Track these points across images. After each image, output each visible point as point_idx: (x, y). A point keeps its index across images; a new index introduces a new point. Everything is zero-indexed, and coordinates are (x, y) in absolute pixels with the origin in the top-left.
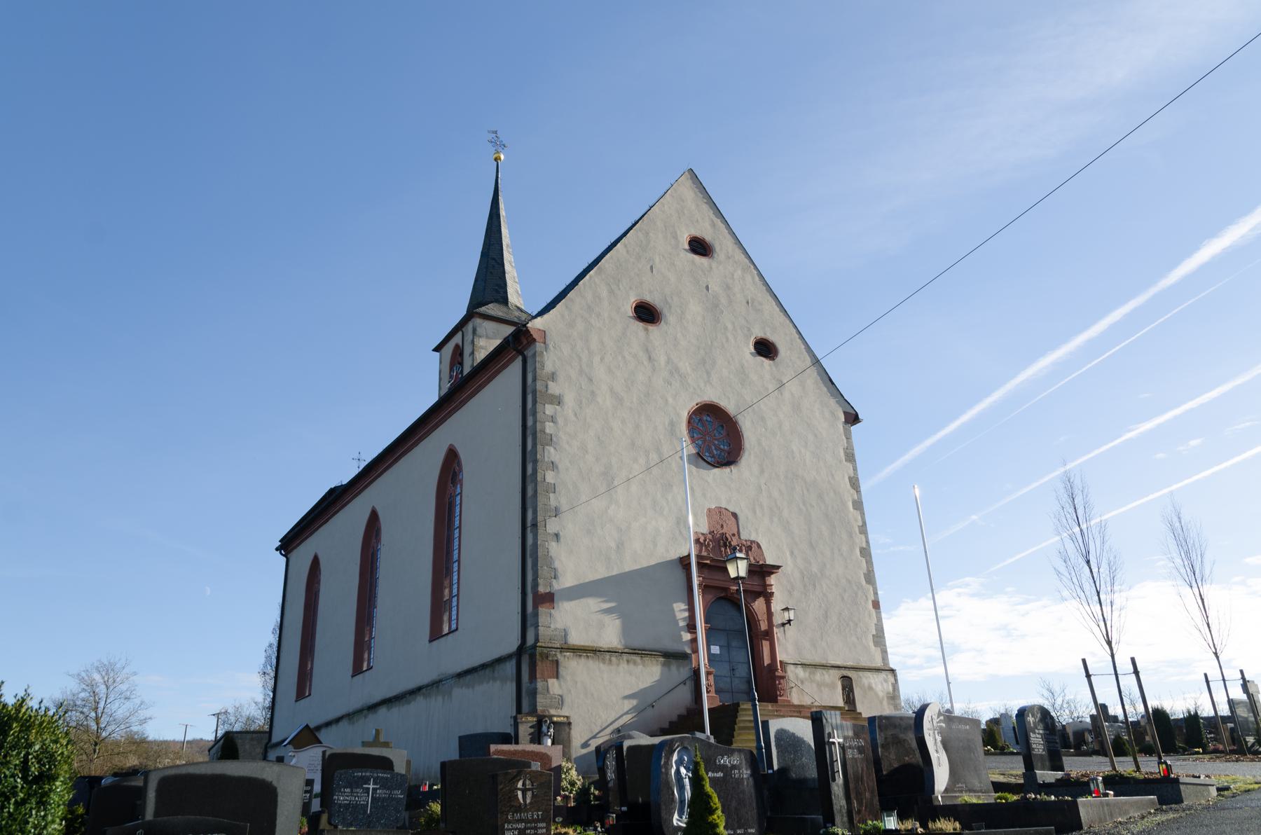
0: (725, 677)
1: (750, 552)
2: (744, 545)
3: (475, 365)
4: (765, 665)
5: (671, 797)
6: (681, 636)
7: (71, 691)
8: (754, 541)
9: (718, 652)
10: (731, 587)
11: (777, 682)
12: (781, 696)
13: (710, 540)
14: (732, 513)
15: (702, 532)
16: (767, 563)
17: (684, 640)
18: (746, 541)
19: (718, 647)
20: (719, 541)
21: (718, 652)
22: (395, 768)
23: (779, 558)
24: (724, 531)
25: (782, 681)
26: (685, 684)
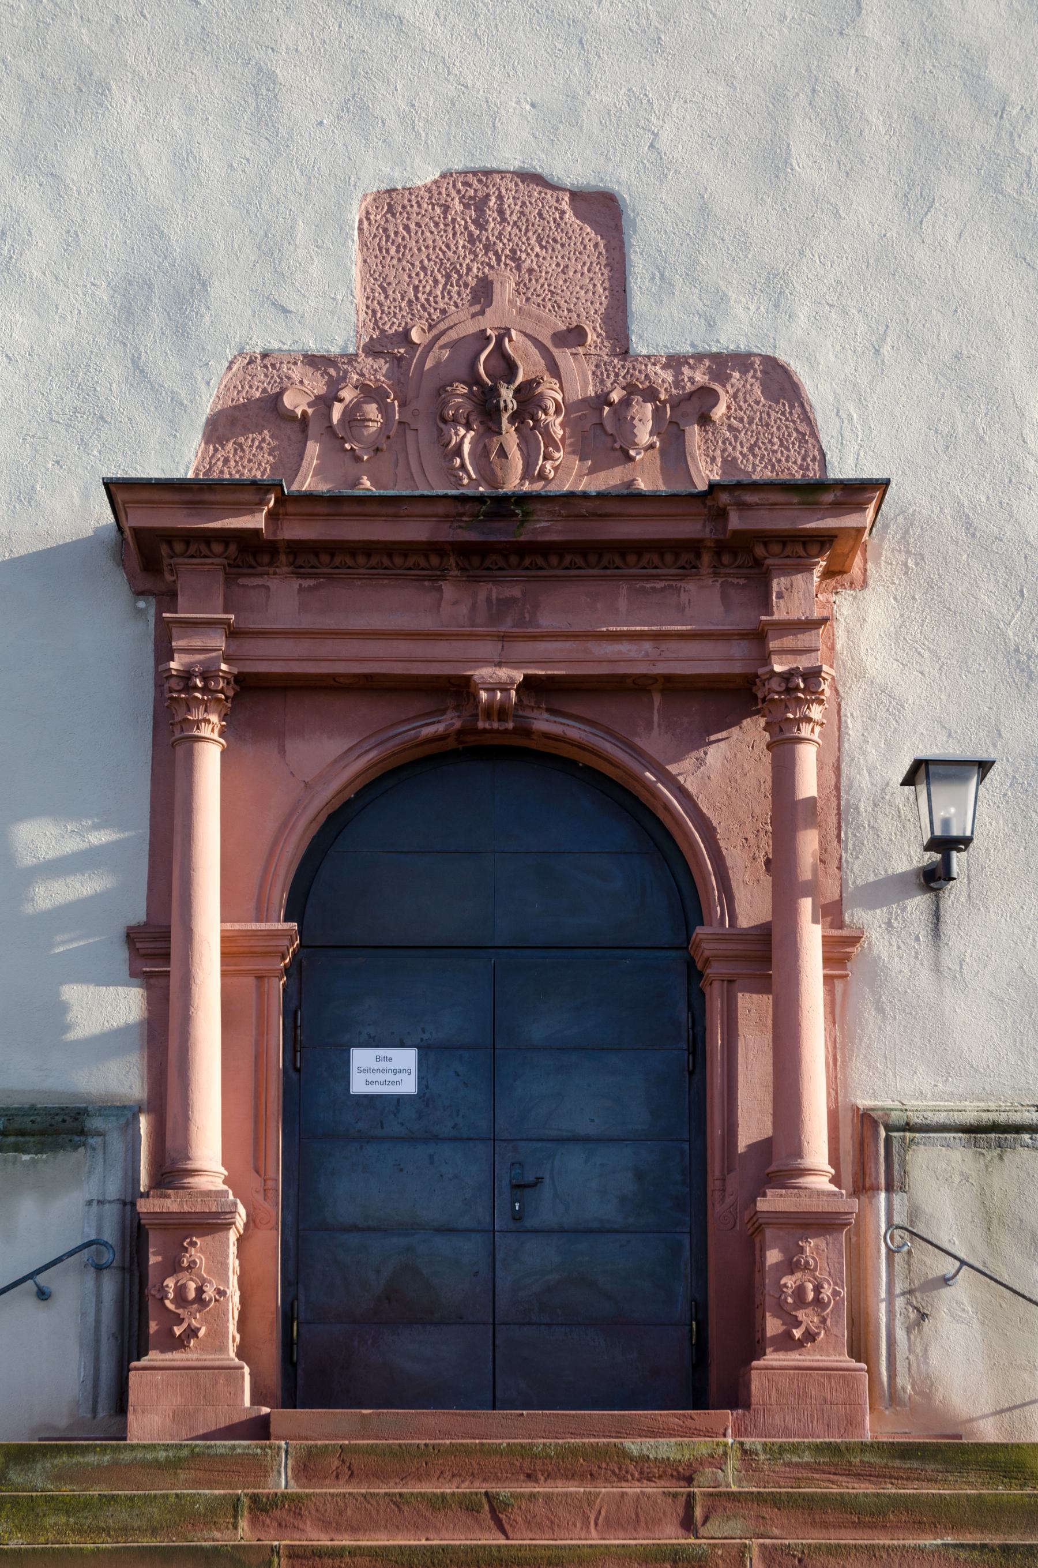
0: (447, 1230)
1: (695, 434)
2: (650, 394)
3: (925, 844)
4: (742, 1148)
5: (601, 1434)
6: (63, 1008)
7: (100, 1134)
8: (742, 361)
9: (409, 1085)
10: (484, 673)
11: (773, 1256)
12: (786, 1342)
13: (369, 393)
14: (578, 197)
15: (313, 345)
16: (834, 473)
17: (71, 1036)
18: (675, 362)
19: (407, 1058)
20: (441, 393)
21: (409, 1085)
22: (765, 1136)
23: (950, 442)
24: (489, 323)
25: (812, 1247)
26: (43, 1295)
